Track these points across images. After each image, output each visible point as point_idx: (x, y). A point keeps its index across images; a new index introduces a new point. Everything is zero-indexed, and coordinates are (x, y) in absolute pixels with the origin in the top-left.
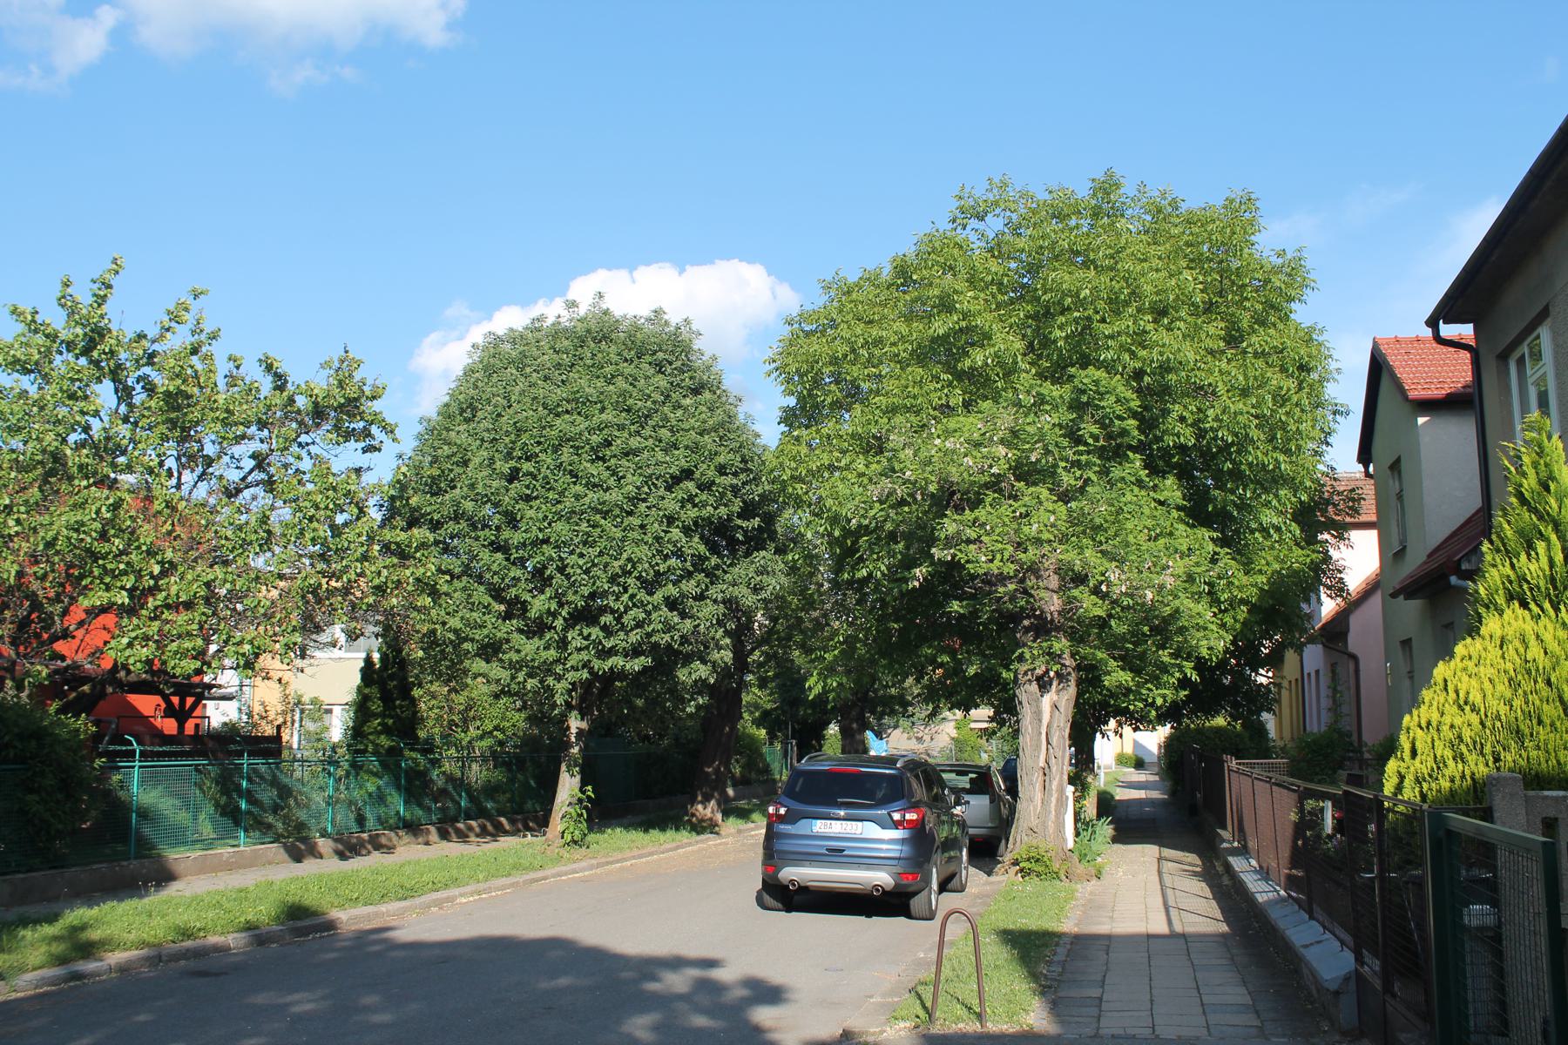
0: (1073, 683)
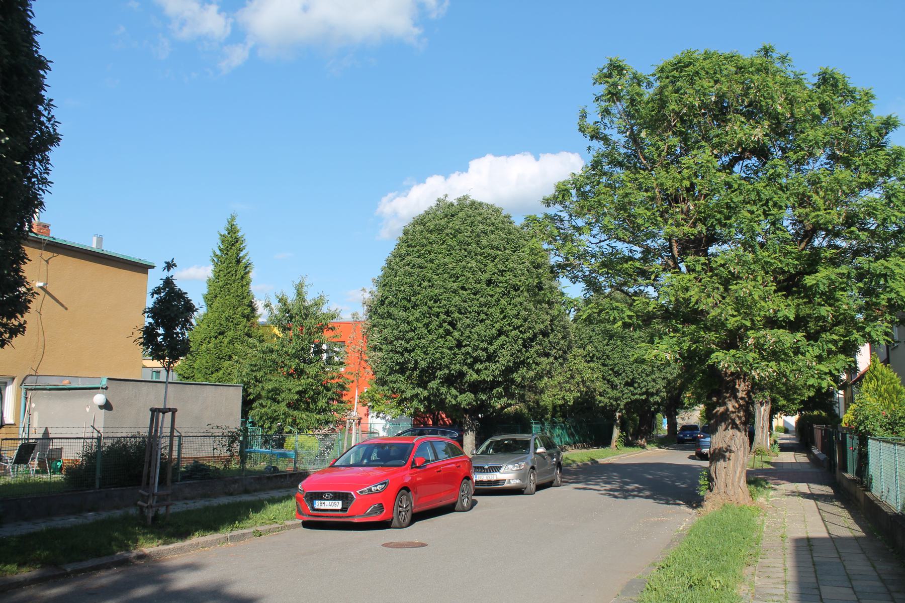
0: (770, 404)
